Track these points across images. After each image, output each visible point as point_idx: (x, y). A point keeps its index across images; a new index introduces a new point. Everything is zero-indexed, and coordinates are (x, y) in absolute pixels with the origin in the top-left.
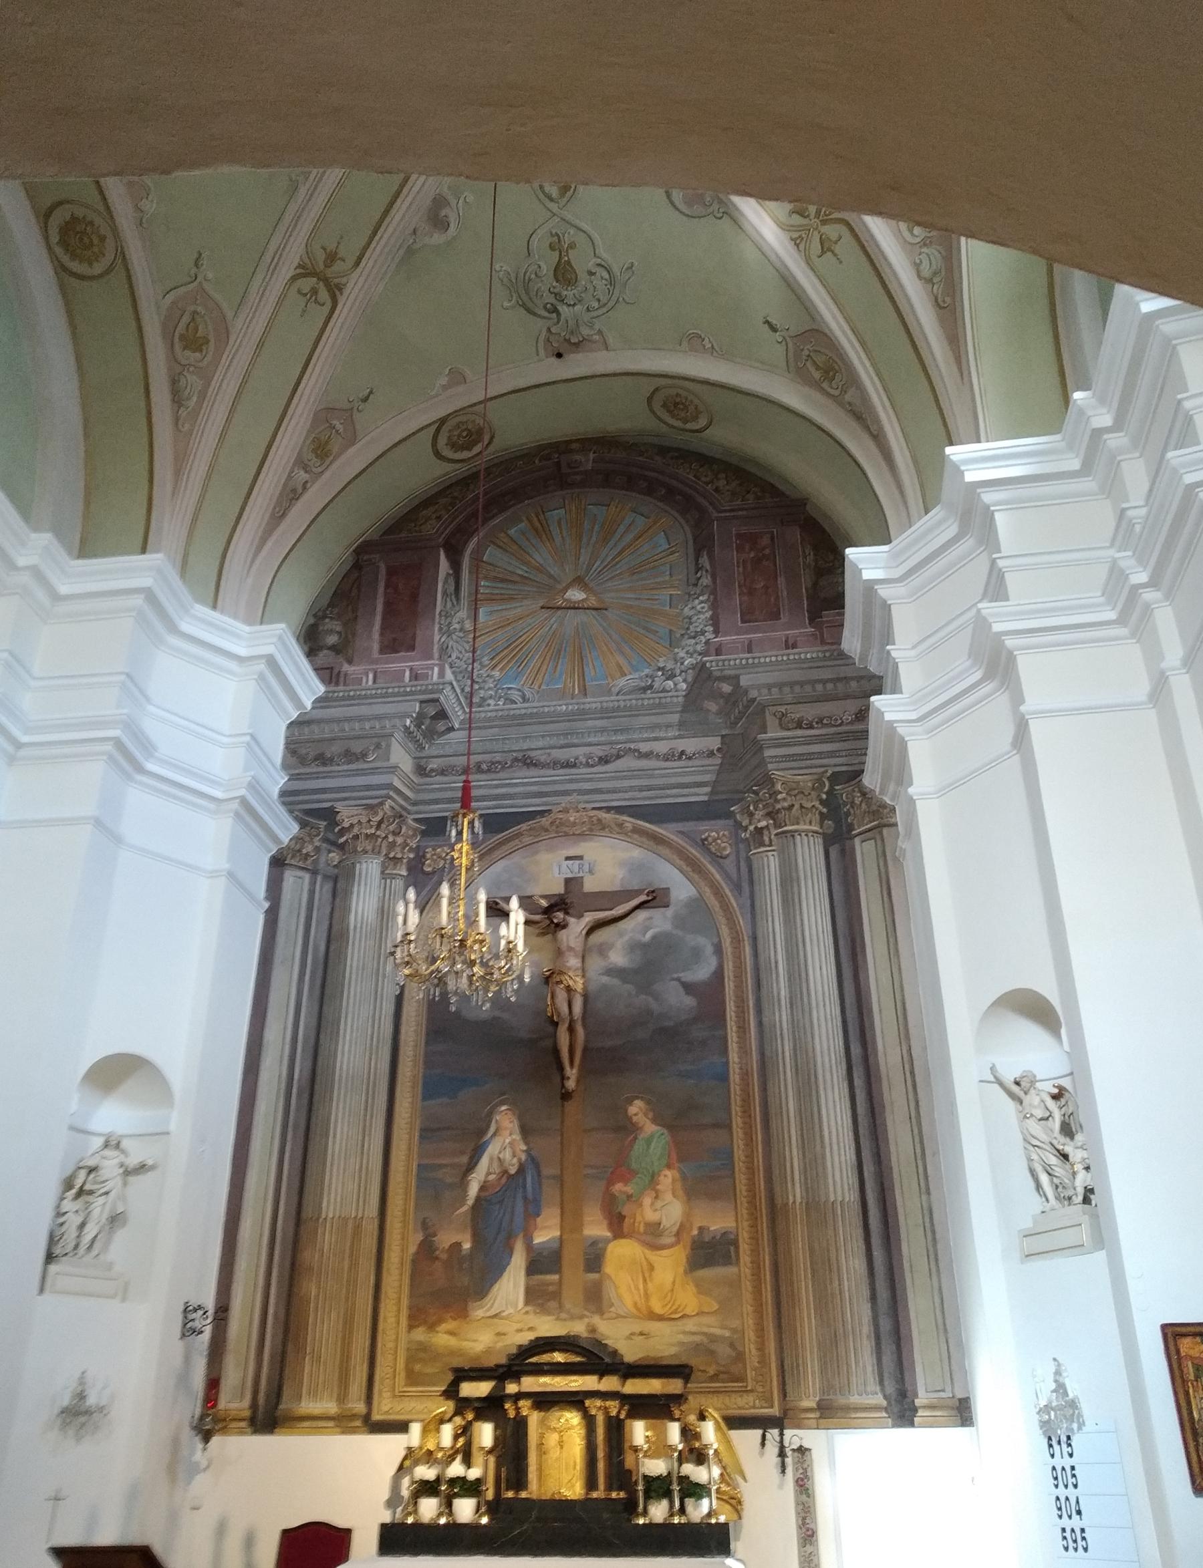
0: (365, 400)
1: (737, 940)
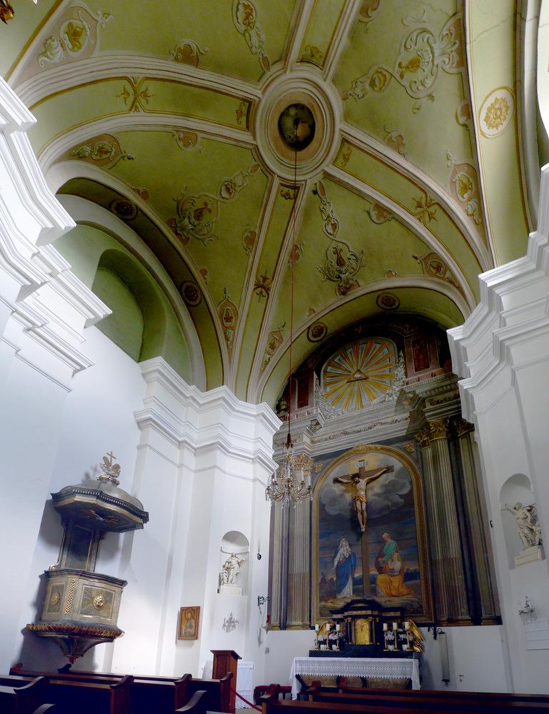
1: (417, 479)
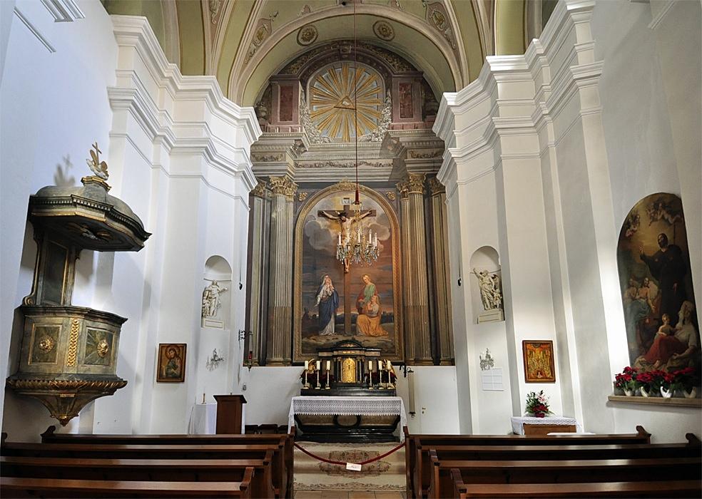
0: (275, 16)
1: (396, 228)
